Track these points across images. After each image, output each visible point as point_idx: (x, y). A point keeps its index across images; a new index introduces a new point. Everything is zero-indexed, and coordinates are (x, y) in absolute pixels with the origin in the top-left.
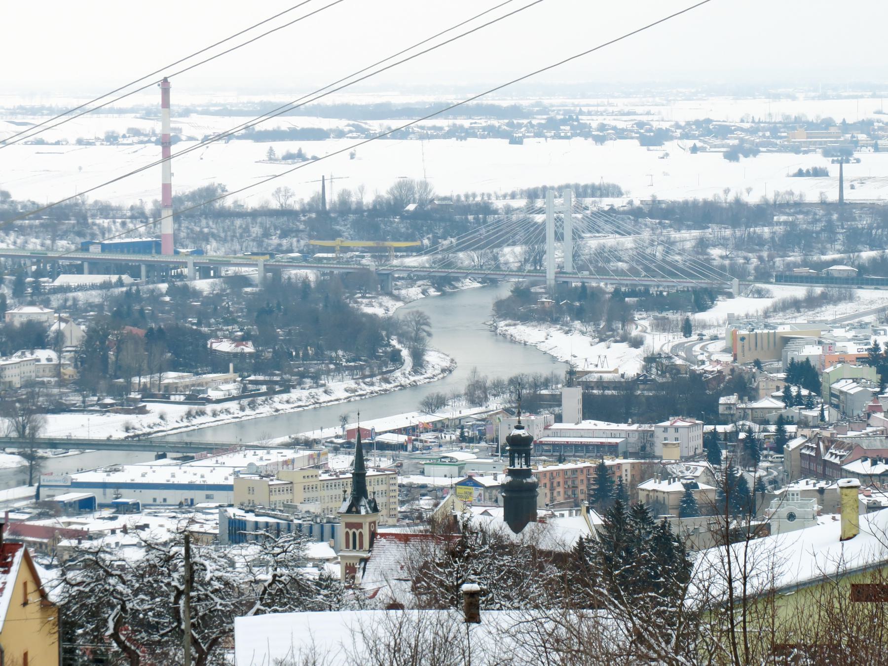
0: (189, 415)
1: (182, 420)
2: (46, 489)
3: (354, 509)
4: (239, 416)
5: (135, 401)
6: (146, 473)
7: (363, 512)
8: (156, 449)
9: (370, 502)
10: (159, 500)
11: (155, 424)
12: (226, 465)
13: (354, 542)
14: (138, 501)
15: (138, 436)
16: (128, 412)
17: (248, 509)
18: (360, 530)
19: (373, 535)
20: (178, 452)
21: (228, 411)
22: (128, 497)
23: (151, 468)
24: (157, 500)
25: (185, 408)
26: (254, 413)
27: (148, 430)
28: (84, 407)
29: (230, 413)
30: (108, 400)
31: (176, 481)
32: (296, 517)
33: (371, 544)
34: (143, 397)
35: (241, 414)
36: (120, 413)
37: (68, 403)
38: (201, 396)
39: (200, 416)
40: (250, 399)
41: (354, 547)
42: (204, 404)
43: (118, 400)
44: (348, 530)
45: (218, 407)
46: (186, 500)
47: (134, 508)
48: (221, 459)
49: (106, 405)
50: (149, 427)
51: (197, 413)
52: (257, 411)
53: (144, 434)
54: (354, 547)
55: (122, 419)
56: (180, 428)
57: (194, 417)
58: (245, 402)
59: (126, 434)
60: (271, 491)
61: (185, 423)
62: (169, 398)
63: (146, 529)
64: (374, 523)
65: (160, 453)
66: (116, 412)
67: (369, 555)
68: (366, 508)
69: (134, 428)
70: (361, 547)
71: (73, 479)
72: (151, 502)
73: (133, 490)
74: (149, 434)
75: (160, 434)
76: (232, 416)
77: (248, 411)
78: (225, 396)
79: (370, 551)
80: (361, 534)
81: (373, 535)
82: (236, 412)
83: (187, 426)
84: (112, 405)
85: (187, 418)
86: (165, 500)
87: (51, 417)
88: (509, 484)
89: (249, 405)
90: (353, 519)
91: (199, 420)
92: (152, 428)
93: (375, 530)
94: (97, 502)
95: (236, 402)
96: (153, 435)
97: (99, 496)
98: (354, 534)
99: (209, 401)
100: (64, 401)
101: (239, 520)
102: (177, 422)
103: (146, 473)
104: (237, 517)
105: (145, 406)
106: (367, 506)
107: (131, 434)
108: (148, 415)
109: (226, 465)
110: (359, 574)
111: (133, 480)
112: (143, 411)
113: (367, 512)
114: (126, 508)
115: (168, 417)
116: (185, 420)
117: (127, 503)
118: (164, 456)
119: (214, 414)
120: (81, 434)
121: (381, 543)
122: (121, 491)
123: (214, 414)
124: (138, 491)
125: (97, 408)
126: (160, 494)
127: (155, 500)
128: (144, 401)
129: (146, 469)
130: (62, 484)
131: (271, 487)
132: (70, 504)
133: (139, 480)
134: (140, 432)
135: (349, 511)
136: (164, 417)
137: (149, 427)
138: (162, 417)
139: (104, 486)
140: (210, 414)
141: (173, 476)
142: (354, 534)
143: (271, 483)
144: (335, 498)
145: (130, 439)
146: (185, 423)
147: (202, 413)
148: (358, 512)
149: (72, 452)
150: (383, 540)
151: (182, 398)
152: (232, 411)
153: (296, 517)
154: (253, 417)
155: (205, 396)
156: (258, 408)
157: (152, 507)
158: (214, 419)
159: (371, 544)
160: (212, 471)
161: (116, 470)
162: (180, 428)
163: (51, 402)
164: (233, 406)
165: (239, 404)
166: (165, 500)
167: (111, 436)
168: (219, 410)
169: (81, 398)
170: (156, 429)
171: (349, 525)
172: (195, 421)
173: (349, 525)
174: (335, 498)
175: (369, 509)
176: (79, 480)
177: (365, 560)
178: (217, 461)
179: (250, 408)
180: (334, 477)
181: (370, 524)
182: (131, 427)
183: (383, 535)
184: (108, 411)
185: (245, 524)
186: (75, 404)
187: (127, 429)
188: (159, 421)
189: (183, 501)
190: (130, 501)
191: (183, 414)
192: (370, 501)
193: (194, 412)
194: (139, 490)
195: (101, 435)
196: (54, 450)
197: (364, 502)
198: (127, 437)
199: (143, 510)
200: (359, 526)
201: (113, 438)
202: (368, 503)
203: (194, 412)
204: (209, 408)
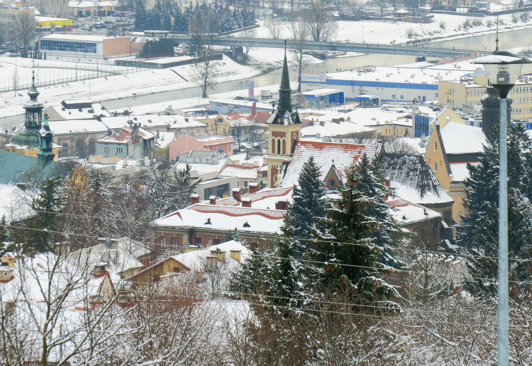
0: (466, 25)
1: (459, 29)
2: (306, 84)
3: (279, 121)
4: (511, 26)
5: (424, 11)
6: (414, 75)
7: (286, 123)
8: (417, 53)
9: (292, 116)
10: (398, 97)
11: (435, 32)
12: (461, 69)
13: (279, 148)
14: (377, 97)
15: (419, 41)
16: (415, 21)
17: (435, 108)
18: (284, 138)
19: (295, 143)
20: (434, 56)
21: (501, 22)
22: (370, 94)
23: (398, 70)
24: (404, 97)
25: (464, 19)
26: (525, 24)
27: (428, 37)
28: (382, 16)
29: (503, 24)
30: (402, 11)
31: (412, 81)
32: (472, 116)
33: (293, 150)
34: (433, 9)
35: (513, 25)
36: (409, 22)
37: (367, 12)
38: (481, 9)
39: (476, 25)
40: (523, 13)
41: (279, 153)
42: (482, 16)
43: (411, 10)
44: (274, 137)
45: (493, 19)
46: (419, 97)
47: (374, 103)
48: (459, 64)
49: (400, 15)
50: (430, 34)
51: (474, 23)
52: (528, 23)
53: (424, 40)
54: (279, 153)
55: (405, 26)
56: (457, 35)
57: (471, 27)
58: (518, 15)
59: (409, 40)
60: (468, 93)
61: (462, 31)
62: (455, 10)
63: (341, 122)
64: (297, 132)
65: (419, 57)
66: (406, 21)
67: (290, 159)
68: (289, 120)
69: (416, 35)
70: (284, 152)
71: (328, 77)
72: (391, 98)
73: (376, 88)
74: (429, 40)
75: (438, 40)
76: (505, 26)
77: (520, 23)
78: (503, 9)
79: (291, 156)
80: (284, 140)
81: (295, 143)
82: (509, 23)
83: (463, 34)
84: (404, 14)
85: (465, 27)
86: (402, 97)
87: (341, 24)
88: (487, 100)
89: (521, 17)
90: (278, 129)
91: (475, 29)
92: (432, 35)
93: (297, 138)
94: (345, 96)
95: (511, 15)
96: (432, 41)
97: (348, 92)
98: (279, 141)
99: (487, 13)
100: (363, 10)
101: (423, 117)
102: (455, 30)
103: (414, 75)
104: (422, 115)
105: (432, 17)
106: (290, 118)
107: (413, 40)
108: (431, 24)
109: (461, 69)
110: (280, 176)
111: (378, 80)
112: (427, 20)
113: (289, 124)
114: (367, 102)
115: (447, 26)
116: (462, 29)
117: (368, 99)
118: (423, 59)
119: (489, 25)
120: (356, 39)
121: (301, 150)
122: (365, 88)
123: (489, 25)
124: (380, 88)
125: (392, 17)
126: (398, 92)
127: (394, 96)
128: (432, 12)
129: (394, 70)
130: (319, 81)
131: (468, 90)
132: (322, 98)
133: (383, 79)
134: (421, 38)
135: (275, 122)
136: (444, 25)
137: (430, 34)
138: (442, 26)
139: (353, 83)
140: (486, 24)
141: (412, 77)
142: (279, 141)
143: (468, 86)
144: (524, 100)
145: (411, 44)
146: (462, 31)
147: (479, 24)
148: (282, 123)
149: (349, 54)
150: (303, 147)
151: (466, 10)
152: (505, 22)
153: (472, 116)
154: (523, 28)
155: (485, 9)
156: (529, 20)
157: (391, 103)
158: (489, 29)
159: (293, 150)
160: (447, 74)
161: (368, 71)
162: (457, 35)
163: (354, 10)
164: (507, 18)
165: (513, 16)
166: (402, 97)
167: (394, 41)
168: (494, 21)
169: (379, 8)
170: (435, 36)
171: (275, 134)
172: (471, 30)
173: (275, 134)
174: (524, 100)
175: (291, 121)
176: (334, 78)
177: (287, 163)
178: (455, 65)
179: (522, 20)
180: (524, 83)
181: (292, 133)
182: (413, 34)
183: (303, 143)
184: (400, 20)
185: (428, 120)
186: (374, 13)
187: (410, 36)
188: (439, 29)
189: (417, 98)
190: (371, 97)
191: (461, 24)
192: (293, 114)
193: (471, 23)
194: (381, 88)
195: (385, 41)
196: (333, 52)
197: (287, 114)
198: (408, 43)
199: (381, 104)
200: (283, 134)
201: (396, 43)
202: (291, 116)
203: (471, 23)
204: (485, 20)
